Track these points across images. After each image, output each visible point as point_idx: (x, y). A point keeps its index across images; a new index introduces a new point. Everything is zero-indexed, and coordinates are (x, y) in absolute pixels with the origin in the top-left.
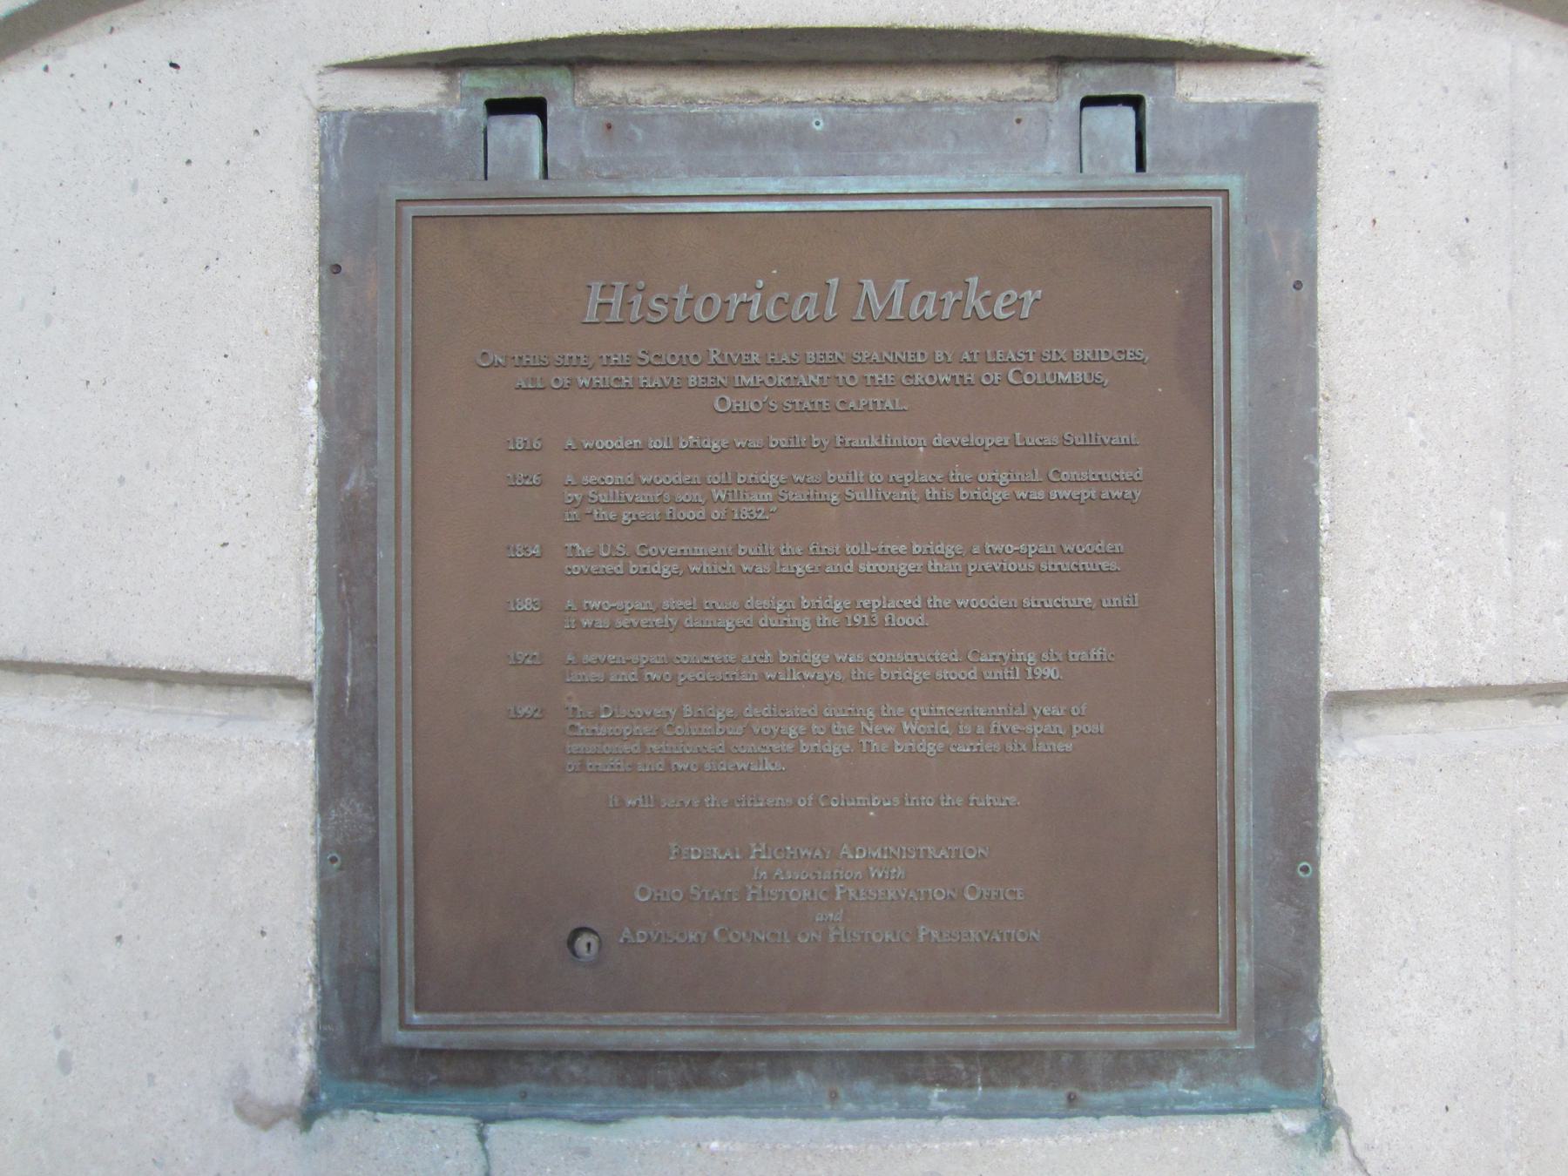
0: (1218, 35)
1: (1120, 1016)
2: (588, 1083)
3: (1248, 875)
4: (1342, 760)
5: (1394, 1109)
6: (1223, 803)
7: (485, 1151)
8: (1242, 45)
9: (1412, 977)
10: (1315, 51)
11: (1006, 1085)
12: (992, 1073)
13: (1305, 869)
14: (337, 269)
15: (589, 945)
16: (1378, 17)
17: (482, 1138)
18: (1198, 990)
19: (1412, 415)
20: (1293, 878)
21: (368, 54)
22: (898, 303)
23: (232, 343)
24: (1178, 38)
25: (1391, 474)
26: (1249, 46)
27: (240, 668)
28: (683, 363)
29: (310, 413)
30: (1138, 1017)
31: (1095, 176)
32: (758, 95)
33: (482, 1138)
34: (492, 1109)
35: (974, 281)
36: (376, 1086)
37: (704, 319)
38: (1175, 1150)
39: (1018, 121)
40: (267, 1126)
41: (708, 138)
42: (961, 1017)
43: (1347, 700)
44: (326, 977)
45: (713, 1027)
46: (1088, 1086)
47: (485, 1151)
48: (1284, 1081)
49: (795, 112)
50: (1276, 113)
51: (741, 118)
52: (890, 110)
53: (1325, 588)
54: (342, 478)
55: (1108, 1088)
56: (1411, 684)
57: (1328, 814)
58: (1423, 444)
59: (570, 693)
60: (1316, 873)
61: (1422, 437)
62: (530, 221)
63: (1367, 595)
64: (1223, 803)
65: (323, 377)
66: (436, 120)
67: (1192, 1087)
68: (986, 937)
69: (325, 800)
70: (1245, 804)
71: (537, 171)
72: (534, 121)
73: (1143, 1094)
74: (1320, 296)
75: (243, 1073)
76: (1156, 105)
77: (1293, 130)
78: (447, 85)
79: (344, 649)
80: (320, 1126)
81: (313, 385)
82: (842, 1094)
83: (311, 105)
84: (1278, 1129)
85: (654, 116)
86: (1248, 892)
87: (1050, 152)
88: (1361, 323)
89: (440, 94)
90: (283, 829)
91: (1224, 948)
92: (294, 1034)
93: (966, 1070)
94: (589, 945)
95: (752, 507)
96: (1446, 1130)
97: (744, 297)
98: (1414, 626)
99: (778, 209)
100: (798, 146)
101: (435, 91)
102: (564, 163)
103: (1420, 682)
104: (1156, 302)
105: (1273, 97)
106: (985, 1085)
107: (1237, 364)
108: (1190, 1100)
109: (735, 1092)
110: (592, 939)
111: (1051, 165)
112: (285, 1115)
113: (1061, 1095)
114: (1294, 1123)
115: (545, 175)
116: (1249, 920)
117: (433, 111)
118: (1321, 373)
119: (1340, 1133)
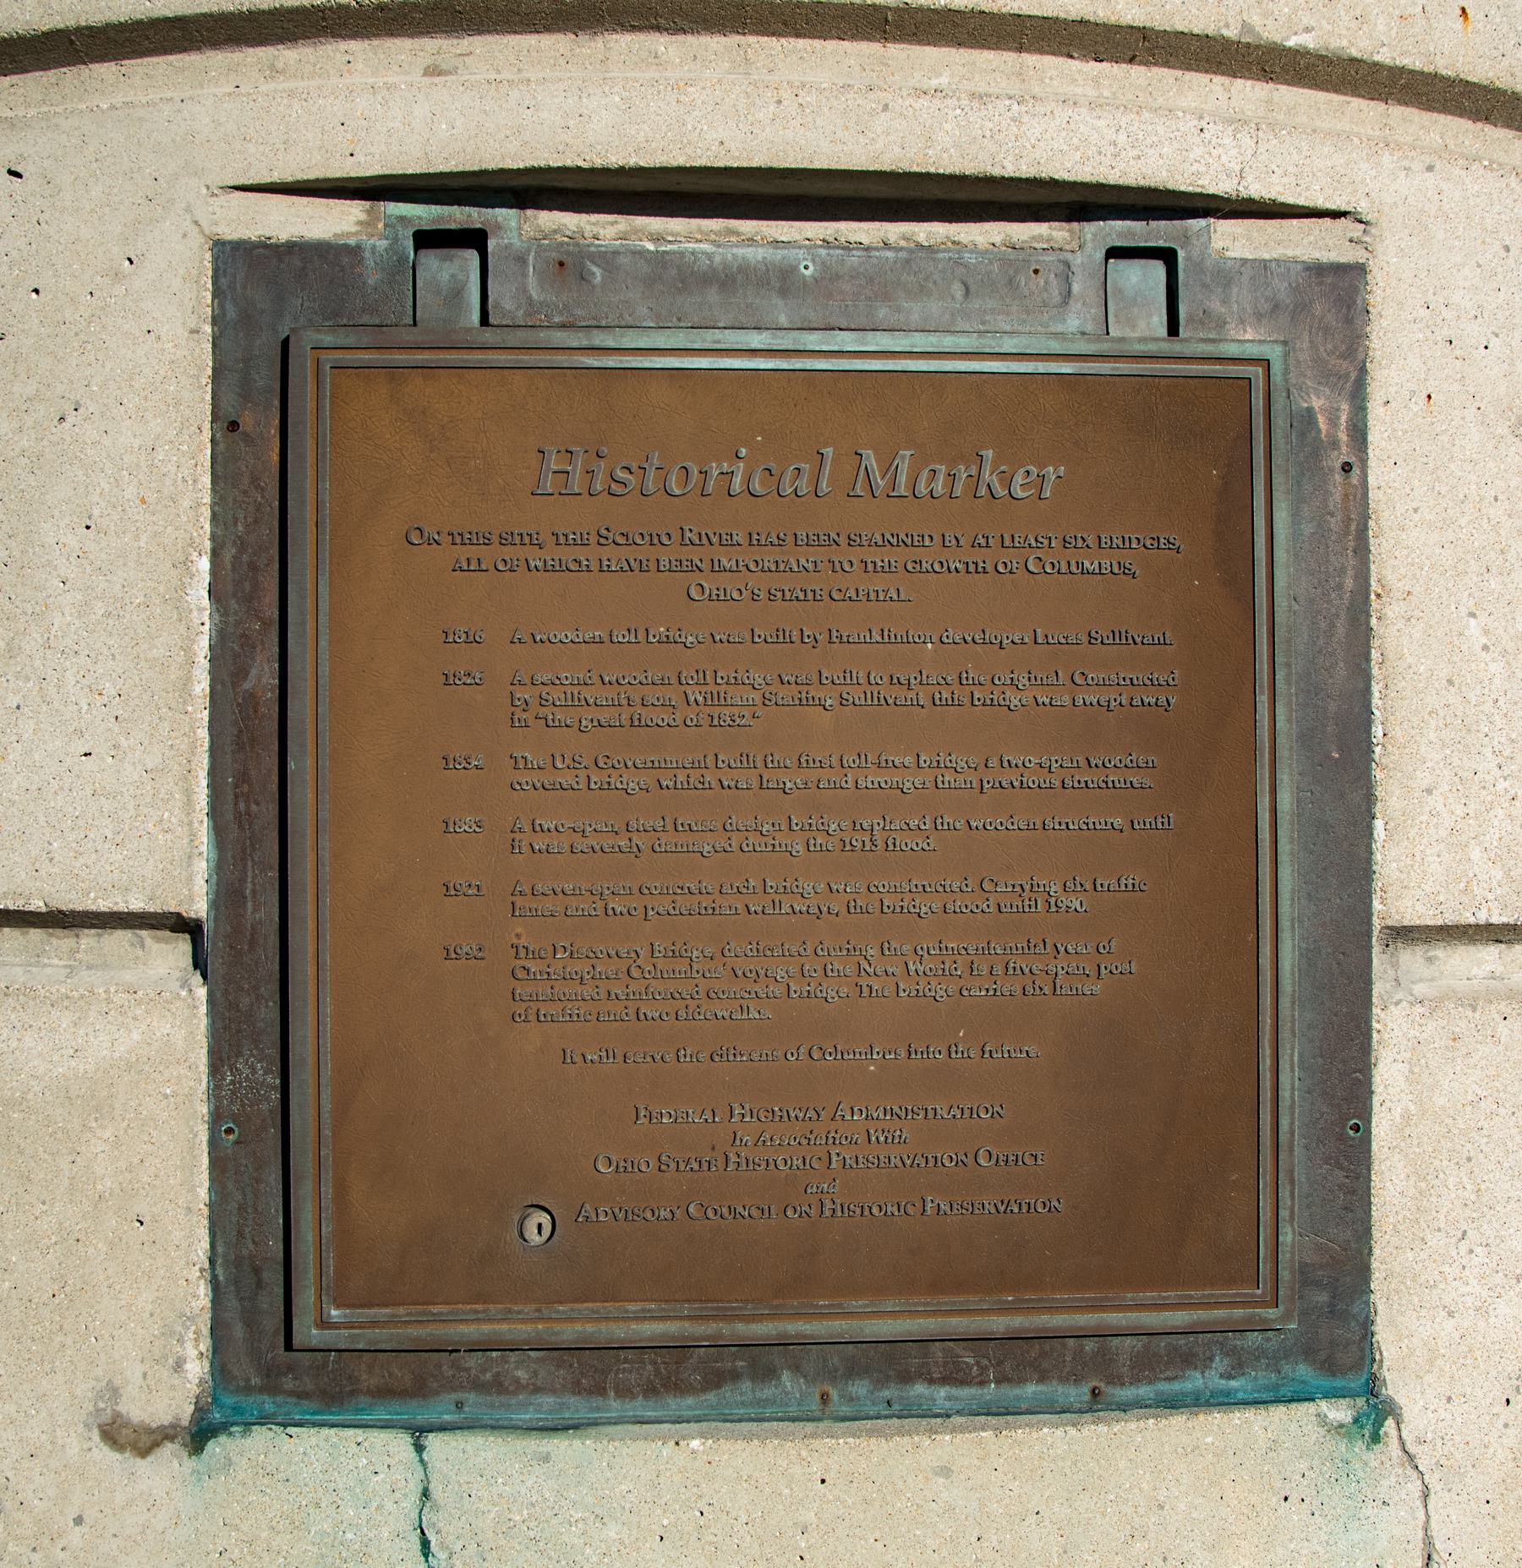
0: (1256, 189)
1: (1149, 1295)
2: (537, 1390)
3: (1292, 1133)
4: (1397, 1004)
5: (1449, 1399)
6: (1266, 1050)
7: (422, 1460)
8: (1281, 199)
9: (1471, 1251)
10: (1363, 207)
11: (1022, 1381)
12: (1007, 1366)
13: (1356, 1128)
14: (233, 426)
15: (540, 1226)
16: (1430, 168)
17: (419, 1448)
18: (1238, 1262)
19: (1473, 615)
20: (1342, 1137)
21: (275, 177)
22: (903, 478)
23: (96, 512)
24: (1211, 191)
25: (1450, 682)
26: (1291, 200)
27: (103, 905)
28: (654, 540)
29: (199, 594)
30: (1171, 1295)
31: (1122, 340)
32: (738, 234)
33: (419, 1448)
34: (420, 1419)
35: (989, 454)
36: (280, 1399)
37: (678, 492)
38: (1209, 1440)
39: (1036, 272)
40: (144, 1453)
41: (675, 277)
42: (973, 1300)
43: (1404, 934)
44: (220, 1271)
45: (689, 1318)
46: (1116, 1380)
47: (422, 1460)
48: (1330, 1367)
49: (780, 253)
50: (1319, 270)
51: (717, 259)
52: (889, 254)
53: (1378, 809)
54: (240, 674)
55: (1136, 1381)
56: (1472, 920)
57: (1380, 1066)
58: (1485, 648)
59: (519, 930)
60: (1368, 1132)
61: (1484, 640)
62: (471, 374)
63: (1424, 818)
64: (1266, 1050)
65: (215, 554)
66: (355, 251)
67: (1230, 1377)
68: (1002, 1209)
69: (217, 1063)
70: (1291, 1054)
71: (475, 317)
72: (472, 257)
73: (1176, 1386)
74: (1372, 481)
75: (113, 1391)
76: (1187, 259)
77: (1339, 292)
78: (368, 212)
79: (243, 880)
80: (214, 1447)
81: (204, 564)
82: (834, 1395)
83: (202, 232)
84: (1321, 1419)
85: (616, 253)
86: (1291, 1150)
87: (1081, 309)
88: (1416, 510)
89: (360, 223)
90: (166, 1096)
91: (1266, 1215)
92: (181, 1341)
93: (978, 1363)
94: (540, 1226)
95: (735, 710)
96: (1506, 1426)
97: (725, 467)
98: (1476, 854)
99: (762, 366)
100: (784, 292)
101: (353, 219)
102: (508, 305)
103: (1482, 918)
104: (1191, 481)
105: (1318, 255)
106: (998, 1382)
107: (1280, 555)
108: (1228, 1393)
109: (711, 1397)
110: (545, 1219)
111: (1073, 323)
112: (171, 1438)
113: (1085, 1390)
114: (1339, 1412)
115: (485, 320)
116: (1292, 1182)
117: (352, 242)
118: (1372, 567)
119: (1390, 1423)
